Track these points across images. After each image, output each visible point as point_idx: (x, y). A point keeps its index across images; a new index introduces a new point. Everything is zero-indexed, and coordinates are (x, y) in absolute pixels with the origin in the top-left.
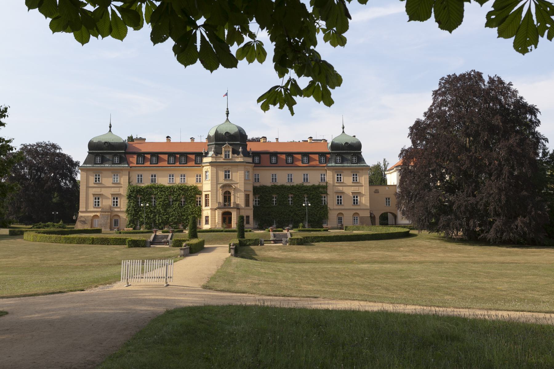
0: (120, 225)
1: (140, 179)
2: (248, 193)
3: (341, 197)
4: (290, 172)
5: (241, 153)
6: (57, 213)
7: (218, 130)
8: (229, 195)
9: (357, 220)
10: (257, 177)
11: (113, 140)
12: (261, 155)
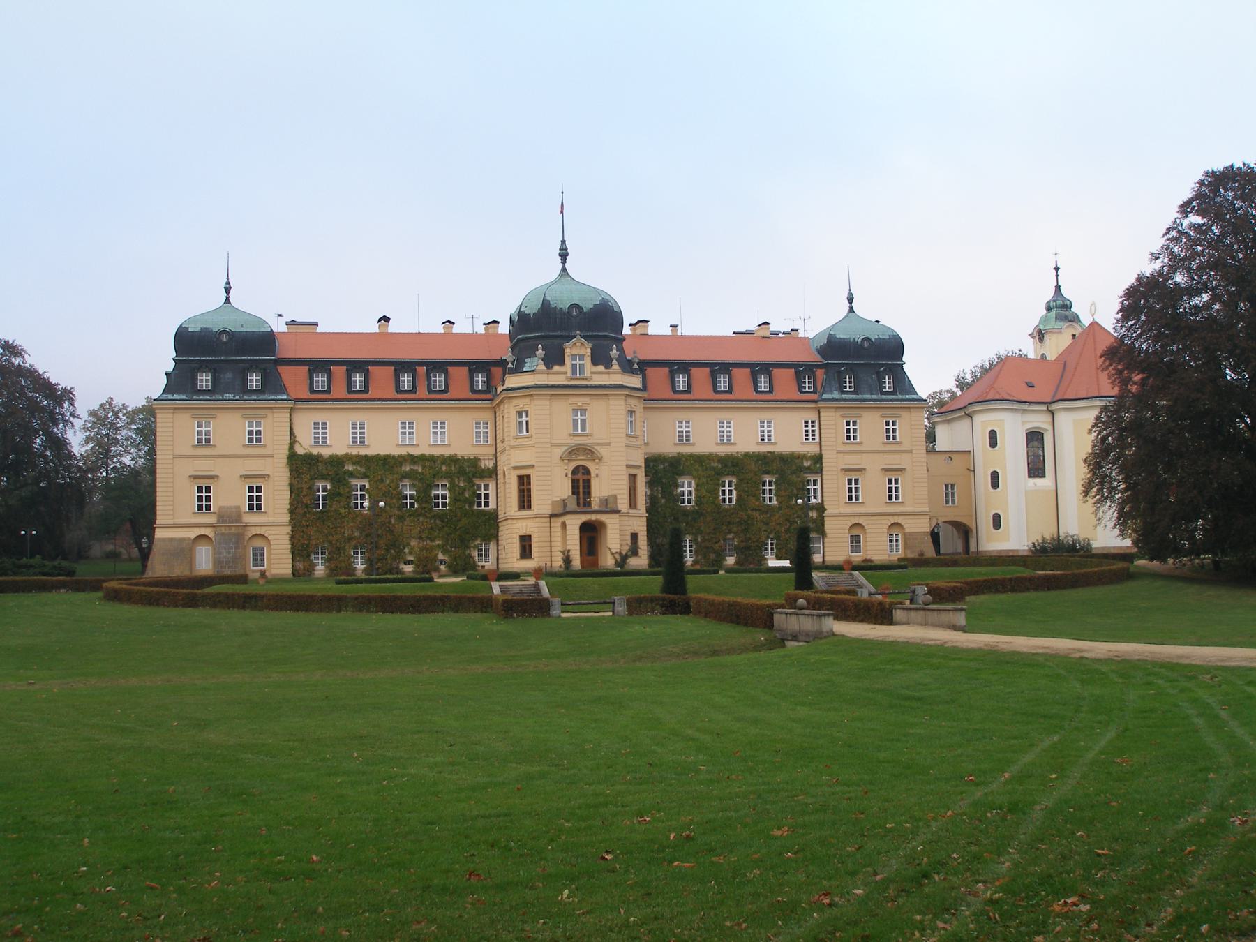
0: (269, 564)
1: (725, 434)
2: (633, 471)
3: (856, 482)
4: (358, 417)
5: (615, 361)
6: (34, 532)
7: (548, 298)
8: (586, 477)
9: (897, 541)
10: (358, 431)
11: (242, 326)
12: (450, 369)
